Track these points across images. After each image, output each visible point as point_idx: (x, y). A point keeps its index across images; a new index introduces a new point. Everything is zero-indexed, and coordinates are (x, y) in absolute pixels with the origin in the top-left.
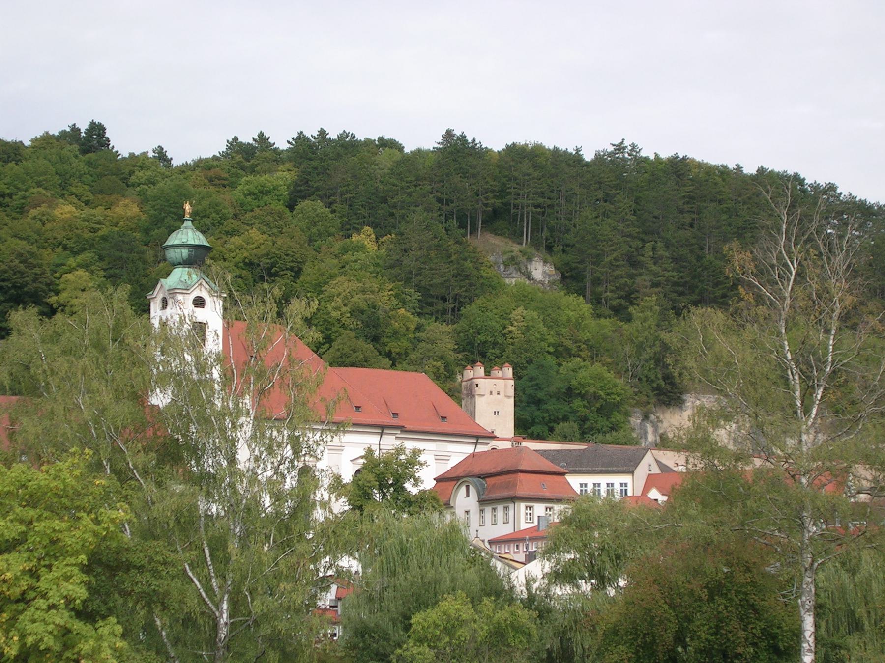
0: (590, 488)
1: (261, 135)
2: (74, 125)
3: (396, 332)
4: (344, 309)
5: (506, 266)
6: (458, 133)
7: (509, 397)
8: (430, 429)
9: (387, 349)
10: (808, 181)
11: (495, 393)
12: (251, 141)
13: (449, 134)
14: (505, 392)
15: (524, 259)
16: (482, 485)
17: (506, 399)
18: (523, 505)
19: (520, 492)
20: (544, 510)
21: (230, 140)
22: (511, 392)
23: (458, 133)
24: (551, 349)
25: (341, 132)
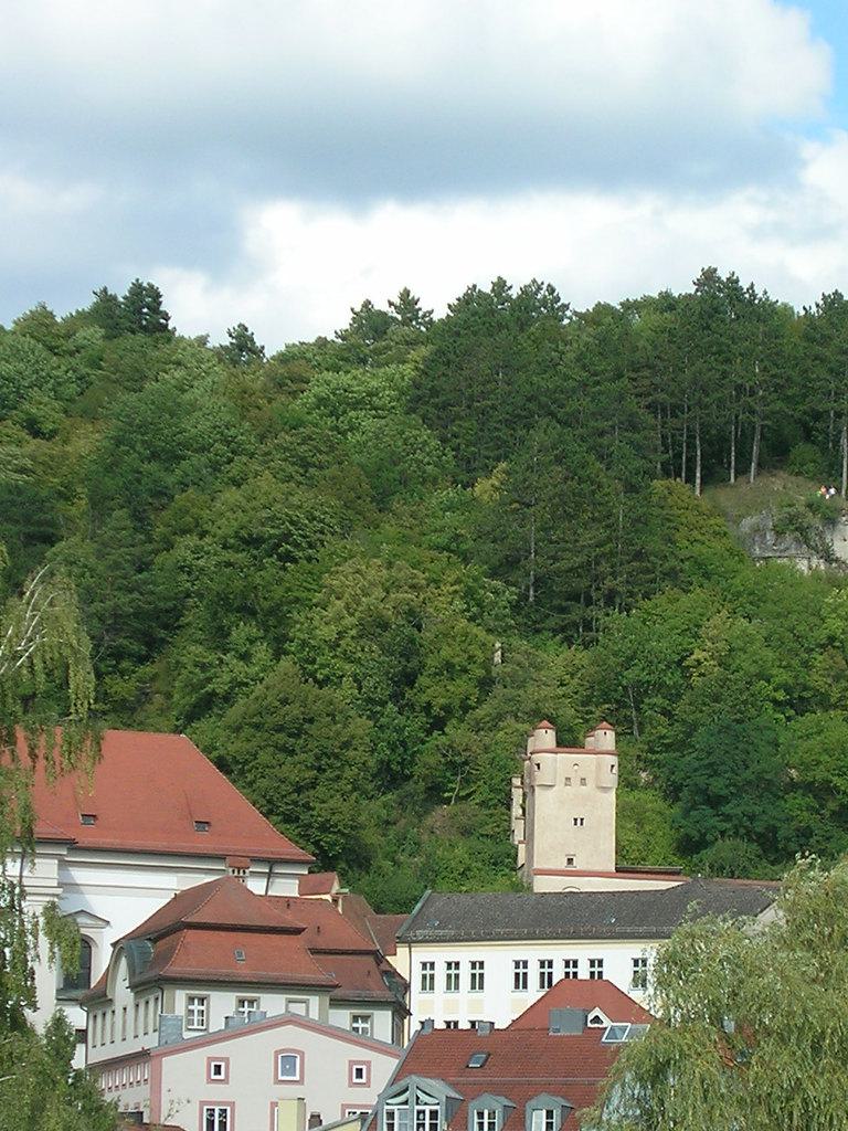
0: (584, 972)
1: (406, 293)
2: (105, 290)
3: (449, 666)
4: (349, 621)
5: (779, 533)
6: (723, 275)
7: (605, 789)
8: (161, 845)
9: (424, 698)
10: (331, 337)
11: (575, 781)
12: (385, 308)
13: (709, 276)
14: (597, 778)
15: (817, 522)
16: (145, 953)
17: (599, 794)
18: (181, 996)
19: (173, 969)
20: (234, 1002)
21: (358, 309)
22: (611, 779)
23: (723, 275)
24: (781, 696)
25: (528, 282)
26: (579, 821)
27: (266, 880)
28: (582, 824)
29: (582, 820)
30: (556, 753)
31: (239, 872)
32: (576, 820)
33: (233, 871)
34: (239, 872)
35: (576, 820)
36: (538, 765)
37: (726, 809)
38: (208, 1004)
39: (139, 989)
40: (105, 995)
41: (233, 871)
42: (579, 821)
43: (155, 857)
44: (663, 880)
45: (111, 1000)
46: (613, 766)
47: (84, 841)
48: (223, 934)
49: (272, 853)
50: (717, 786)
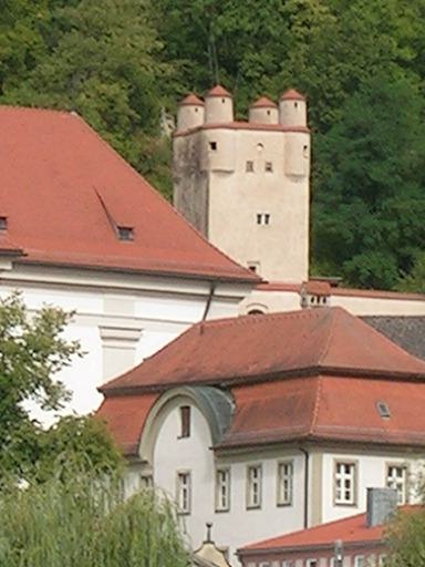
7: (296, 178)
11: (259, 167)
16: (223, 405)
18: (328, 460)
19: (322, 427)
20: (384, 471)
22: (303, 165)
26: (263, 218)
27: (205, 304)
28: (267, 222)
29: (267, 216)
30: (236, 129)
31: (318, 301)
32: (259, 216)
33: (312, 300)
34: (318, 301)
35: (259, 216)
36: (214, 146)
37: (387, 203)
38: (356, 470)
39: (221, 453)
40: (137, 455)
41: (312, 300)
42: (263, 218)
43: (149, 278)
44: (389, 298)
45: (146, 462)
46: (305, 147)
47: (34, 253)
48: (360, 382)
49: (212, 269)
50: (378, 172)
